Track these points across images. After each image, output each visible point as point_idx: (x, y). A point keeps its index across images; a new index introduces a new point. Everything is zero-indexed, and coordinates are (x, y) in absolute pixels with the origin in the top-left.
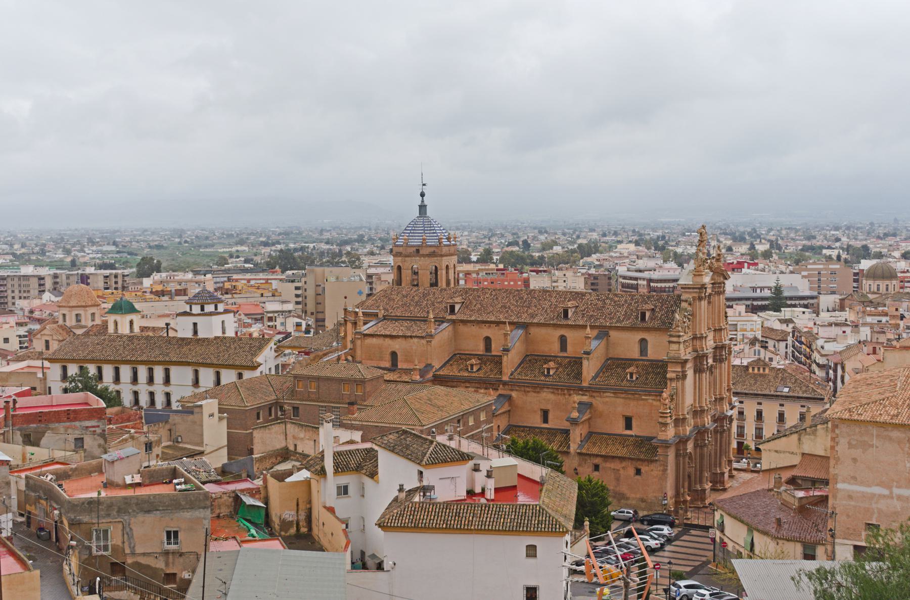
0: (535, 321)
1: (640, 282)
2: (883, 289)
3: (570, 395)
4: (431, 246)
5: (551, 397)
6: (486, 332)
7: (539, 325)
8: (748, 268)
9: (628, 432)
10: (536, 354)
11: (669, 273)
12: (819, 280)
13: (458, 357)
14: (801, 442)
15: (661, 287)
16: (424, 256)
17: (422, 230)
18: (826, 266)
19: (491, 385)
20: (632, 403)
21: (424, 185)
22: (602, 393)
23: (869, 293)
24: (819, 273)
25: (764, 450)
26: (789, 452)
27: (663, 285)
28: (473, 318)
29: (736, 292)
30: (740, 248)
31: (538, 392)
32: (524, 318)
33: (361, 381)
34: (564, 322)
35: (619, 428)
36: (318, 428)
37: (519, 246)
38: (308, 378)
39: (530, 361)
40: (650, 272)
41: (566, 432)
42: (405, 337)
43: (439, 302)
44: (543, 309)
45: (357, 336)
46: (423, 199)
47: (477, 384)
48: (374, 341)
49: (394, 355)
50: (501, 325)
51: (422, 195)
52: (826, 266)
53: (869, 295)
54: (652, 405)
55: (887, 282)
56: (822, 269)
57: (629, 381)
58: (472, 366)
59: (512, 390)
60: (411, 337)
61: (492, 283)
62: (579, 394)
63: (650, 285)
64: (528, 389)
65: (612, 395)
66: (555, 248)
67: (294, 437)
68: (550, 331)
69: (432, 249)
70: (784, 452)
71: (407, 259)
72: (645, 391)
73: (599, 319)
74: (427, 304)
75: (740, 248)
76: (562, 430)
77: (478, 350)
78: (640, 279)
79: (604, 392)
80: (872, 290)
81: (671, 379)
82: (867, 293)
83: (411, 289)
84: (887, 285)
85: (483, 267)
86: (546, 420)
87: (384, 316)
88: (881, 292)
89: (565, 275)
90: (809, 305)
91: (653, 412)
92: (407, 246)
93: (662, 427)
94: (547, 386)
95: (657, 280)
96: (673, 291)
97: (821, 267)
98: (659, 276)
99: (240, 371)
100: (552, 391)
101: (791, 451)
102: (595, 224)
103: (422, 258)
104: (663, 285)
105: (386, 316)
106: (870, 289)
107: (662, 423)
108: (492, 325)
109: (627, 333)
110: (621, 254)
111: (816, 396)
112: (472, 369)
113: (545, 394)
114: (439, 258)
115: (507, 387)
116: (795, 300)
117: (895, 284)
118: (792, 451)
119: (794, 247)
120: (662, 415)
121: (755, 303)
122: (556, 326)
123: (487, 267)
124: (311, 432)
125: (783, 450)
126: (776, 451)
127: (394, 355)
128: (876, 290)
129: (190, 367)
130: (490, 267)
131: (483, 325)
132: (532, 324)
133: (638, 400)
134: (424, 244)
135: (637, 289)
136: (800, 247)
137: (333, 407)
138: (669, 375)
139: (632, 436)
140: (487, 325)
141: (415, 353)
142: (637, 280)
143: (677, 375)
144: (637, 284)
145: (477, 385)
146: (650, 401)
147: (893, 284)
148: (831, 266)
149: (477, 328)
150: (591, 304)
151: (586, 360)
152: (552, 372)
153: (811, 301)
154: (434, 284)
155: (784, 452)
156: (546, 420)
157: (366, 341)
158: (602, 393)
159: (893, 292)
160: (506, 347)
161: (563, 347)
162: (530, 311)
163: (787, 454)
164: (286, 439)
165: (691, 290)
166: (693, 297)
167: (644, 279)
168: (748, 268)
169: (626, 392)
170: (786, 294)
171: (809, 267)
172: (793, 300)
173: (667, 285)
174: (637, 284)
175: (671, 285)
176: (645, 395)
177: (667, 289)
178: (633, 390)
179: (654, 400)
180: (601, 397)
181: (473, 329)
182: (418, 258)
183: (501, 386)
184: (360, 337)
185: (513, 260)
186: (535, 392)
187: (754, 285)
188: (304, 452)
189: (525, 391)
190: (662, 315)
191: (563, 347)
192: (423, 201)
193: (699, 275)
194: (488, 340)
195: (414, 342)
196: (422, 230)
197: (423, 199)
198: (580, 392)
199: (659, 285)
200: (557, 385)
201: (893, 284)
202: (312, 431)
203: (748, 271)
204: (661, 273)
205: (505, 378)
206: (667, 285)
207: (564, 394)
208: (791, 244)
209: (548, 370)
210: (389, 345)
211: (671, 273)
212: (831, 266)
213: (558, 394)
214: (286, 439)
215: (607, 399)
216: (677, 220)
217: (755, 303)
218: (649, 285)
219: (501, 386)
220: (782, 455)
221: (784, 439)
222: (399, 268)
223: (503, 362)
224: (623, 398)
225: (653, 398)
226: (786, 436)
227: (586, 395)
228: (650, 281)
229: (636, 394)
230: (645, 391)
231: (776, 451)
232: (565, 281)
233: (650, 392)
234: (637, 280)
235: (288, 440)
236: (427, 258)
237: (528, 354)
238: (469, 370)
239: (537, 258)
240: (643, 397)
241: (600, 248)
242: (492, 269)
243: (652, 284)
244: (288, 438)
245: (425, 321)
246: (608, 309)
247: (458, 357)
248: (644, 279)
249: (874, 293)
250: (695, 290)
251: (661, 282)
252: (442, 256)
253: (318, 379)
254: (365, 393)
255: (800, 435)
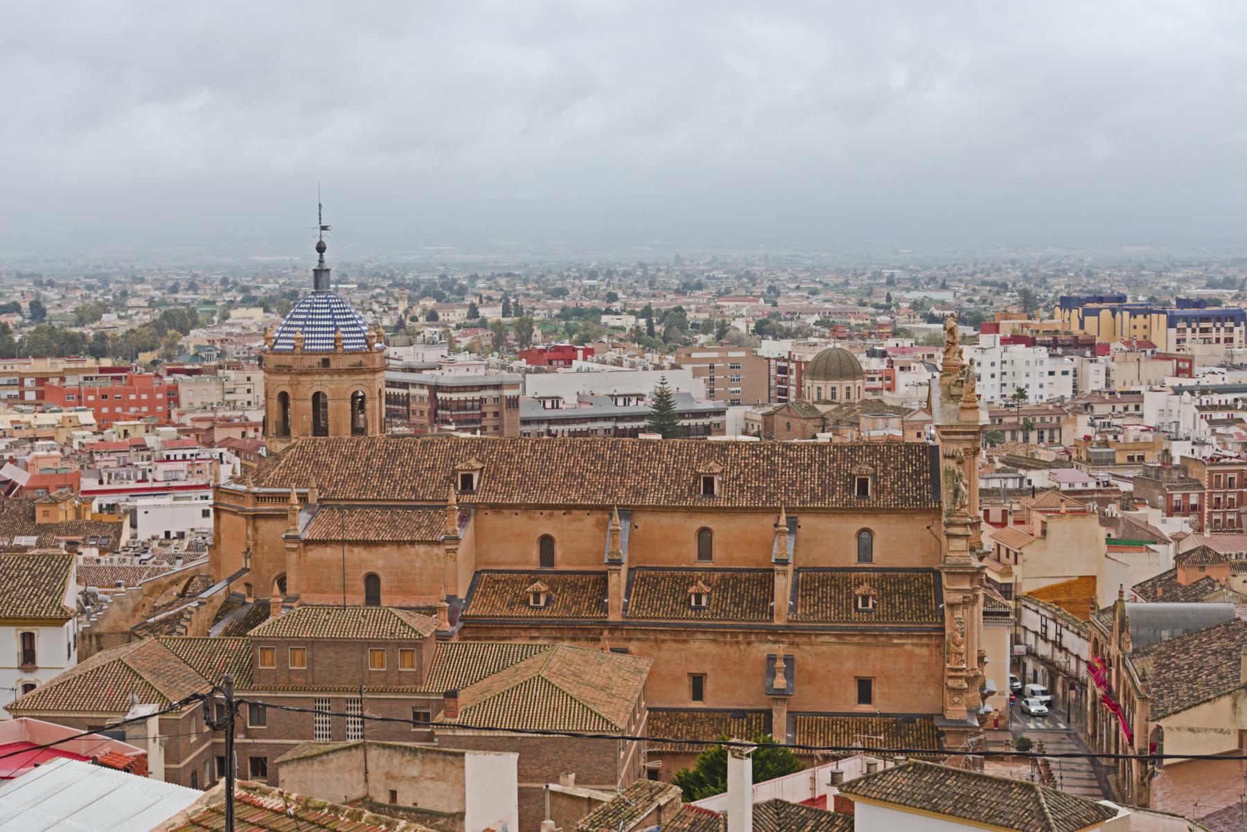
0: (650, 501)
1: (413, 391)
2: (841, 396)
3: (749, 643)
4: (353, 352)
5: (712, 649)
6: (545, 525)
7: (655, 509)
8: (585, 359)
9: (864, 708)
10: (648, 565)
11: (469, 374)
12: (712, 379)
13: (486, 579)
14: (1237, 711)
15: (459, 401)
16: (339, 372)
17: (329, 320)
18: (723, 355)
19: (585, 633)
20: (874, 653)
21: (324, 228)
22: (813, 637)
23: (818, 403)
24: (712, 367)
25: (1169, 728)
26: (1215, 730)
27: (462, 396)
28: (516, 499)
29: (583, 406)
30: (451, 314)
31: (684, 641)
32: (623, 497)
33: (411, 644)
34: (707, 503)
35: (849, 702)
36: (463, 754)
37: (21, 313)
38: (289, 643)
39: (643, 579)
40: (433, 372)
41: (768, 714)
42: (399, 543)
43: (428, 469)
44: (654, 478)
45: (289, 545)
46: (321, 256)
47: (554, 632)
48: (329, 553)
49: (372, 580)
50: (573, 512)
51: (321, 248)
52: (723, 355)
53: (819, 407)
54: (911, 655)
55: (848, 383)
56: (716, 359)
57: (863, 611)
58: (537, 595)
59: (630, 640)
60: (412, 543)
61: (104, 397)
62: (768, 641)
63: (435, 397)
64: (663, 637)
65: (833, 640)
66: (105, 317)
67: (389, 776)
68: (679, 520)
69: (356, 359)
70: (1206, 730)
71: (302, 378)
72: (900, 629)
73: (774, 494)
74: (404, 473)
75: (451, 314)
76: (737, 711)
77: (527, 563)
78: (414, 385)
79: (817, 635)
80: (823, 398)
81: (952, 606)
82: (814, 402)
83: (358, 444)
84: (848, 388)
85: (72, 366)
86: (698, 694)
87: (319, 500)
88: (837, 400)
89: (249, 379)
90: (712, 426)
91: (914, 667)
92: (305, 353)
93: (955, 695)
94: (703, 630)
95: (452, 387)
96: (480, 408)
97: (715, 355)
98: (454, 378)
99: (28, 629)
100: (712, 637)
101: (1219, 727)
102: (132, 267)
103: (336, 377)
104: (462, 396)
105: (324, 499)
106: (819, 395)
107: (954, 689)
108: (556, 512)
109: (833, 520)
110: (243, 328)
111: (996, 610)
112: (537, 601)
113: (697, 644)
114: (368, 377)
115: (618, 634)
116: (689, 418)
117: (861, 385)
118: (1222, 727)
119: (546, 311)
120: (953, 674)
121: (621, 426)
122: (691, 510)
123: (80, 366)
124: (441, 764)
125: (1204, 726)
126: (1191, 730)
127: (372, 580)
128: (829, 398)
129: (13, 629)
130: (86, 366)
131: (538, 512)
132: (642, 509)
133: (884, 646)
134: (340, 350)
135: (407, 404)
136: (556, 312)
137: (347, 700)
138: (949, 598)
139: (874, 715)
140: (546, 512)
141: (421, 574)
142: (407, 388)
143: (964, 597)
144: (408, 395)
145: (554, 634)
146: (910, 647)
147: (857, 385)
148: (731, 354)
149: (525, 518)
150: (746, 465)
151: (781, 576)
152: (704, 602)
153: (715, 419)
154: (320, 429)
155: (1206, 730)
156: (698, 694)
157: (310, 554)
158: (813, 637)
159: (857, 401)
160: (616, 557)
161: (705, 551)
162: (629, 483)
163: (1212, 733)
164: (366, 781)
165: (961, 437)
166: (965, 449)
167: (422, 386)
168: (585, 359)
169: (863, 632)
170: (679, 407)
171: (694, 355)
172: (685, 418)
173: (469, 396)
174: (408, 395)
175: (477, 395)
176: (900, 637)
177: (469, 404)
178: (876, 629)
179: (917, 645)
180: (811, 645)
181: (518, 521)
182: (326, 377)
183: (606, 633)
184: (295, 546)
185: (55, 345)
186: (676, 641)
187: (611, 392)
188: (419, 806)
189: (656, 641)
190: (893, 484)
191: (705, 551)
192: (321, 261)
193: (972, 408)
194: (546, 543)
195: (417, 554)
196: (329, 320)
197: (321, 256)
198: (770, 637)
199: (455, 396)
200: (725, 627)
201: (857, 385)
202: (444, 760)
203: (585, 365)
204: (452, 374)
205: (614, 617)
206: (469, 396)
207: (737, 643)
208: (541, 306)
209: (698, 597)
210: (363, 561)
211: (472, 373)
212: (731, 354)
213: (725, 643)
214: (366, 781)
215: (824, 648)
216: (287, 258)
217: (621, 426)
218: (433, 397)
219: (606, 633)
220: (1202, 736)
221: (1206, 706)
222: (284, 397)
223: (610, 585)
224: (855, 644)
225: (914, 641)
226: (1209, 700)
227: (782, 642)
228: (434, 389)
229: (882, 635)
230: (900, 629)
231: (1191, 730)
232: (249, 391)
233: (908, 630)
234: (407, 388)
235: (371, 784)
236: (345, 377)
237: (634, 566)
238: (531, 603)
239: (92, 340)
240: (895, 641)
241: (201, 318)
242: (91, 370)
243: (439, 395)
244: (371, 777)
245: (443, 507)
246: (784, 473)
247: (486, 579)
248: (422, 386)
249: (826, 402)
250: (969, 437)
251: (458, 392)
252: (374, 371)
253: (313, 643)
254: (420, 668)
255: (1235, 699)
